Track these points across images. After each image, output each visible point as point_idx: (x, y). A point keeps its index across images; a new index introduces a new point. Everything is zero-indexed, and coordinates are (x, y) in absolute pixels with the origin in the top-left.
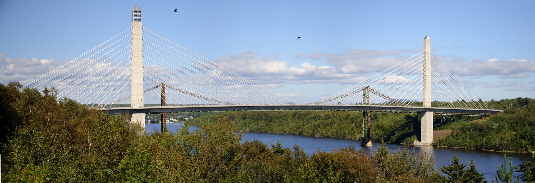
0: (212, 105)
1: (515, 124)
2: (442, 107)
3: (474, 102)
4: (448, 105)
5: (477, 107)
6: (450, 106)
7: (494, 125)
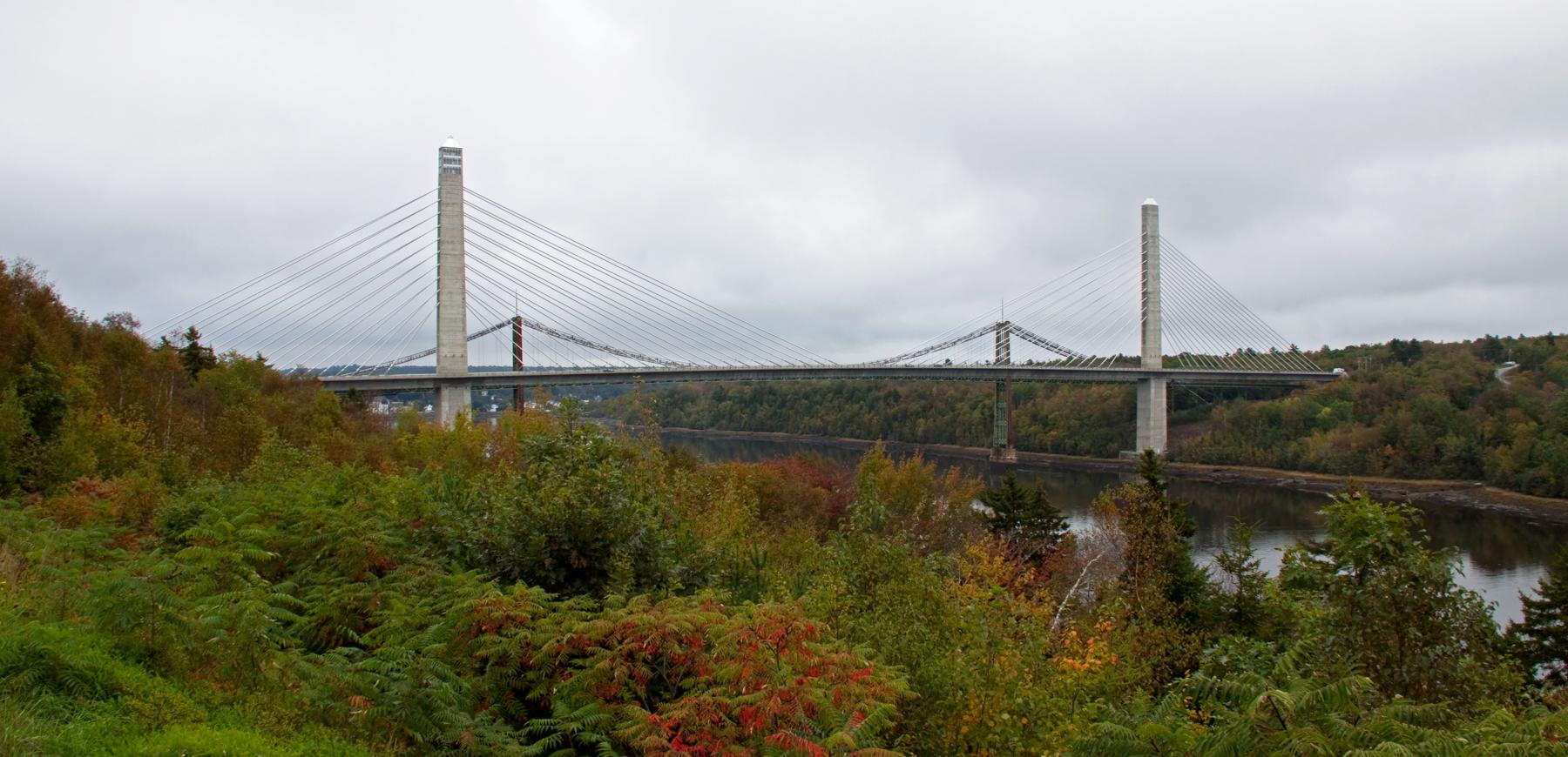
3: (1280, 354)
4: (1205, 361)
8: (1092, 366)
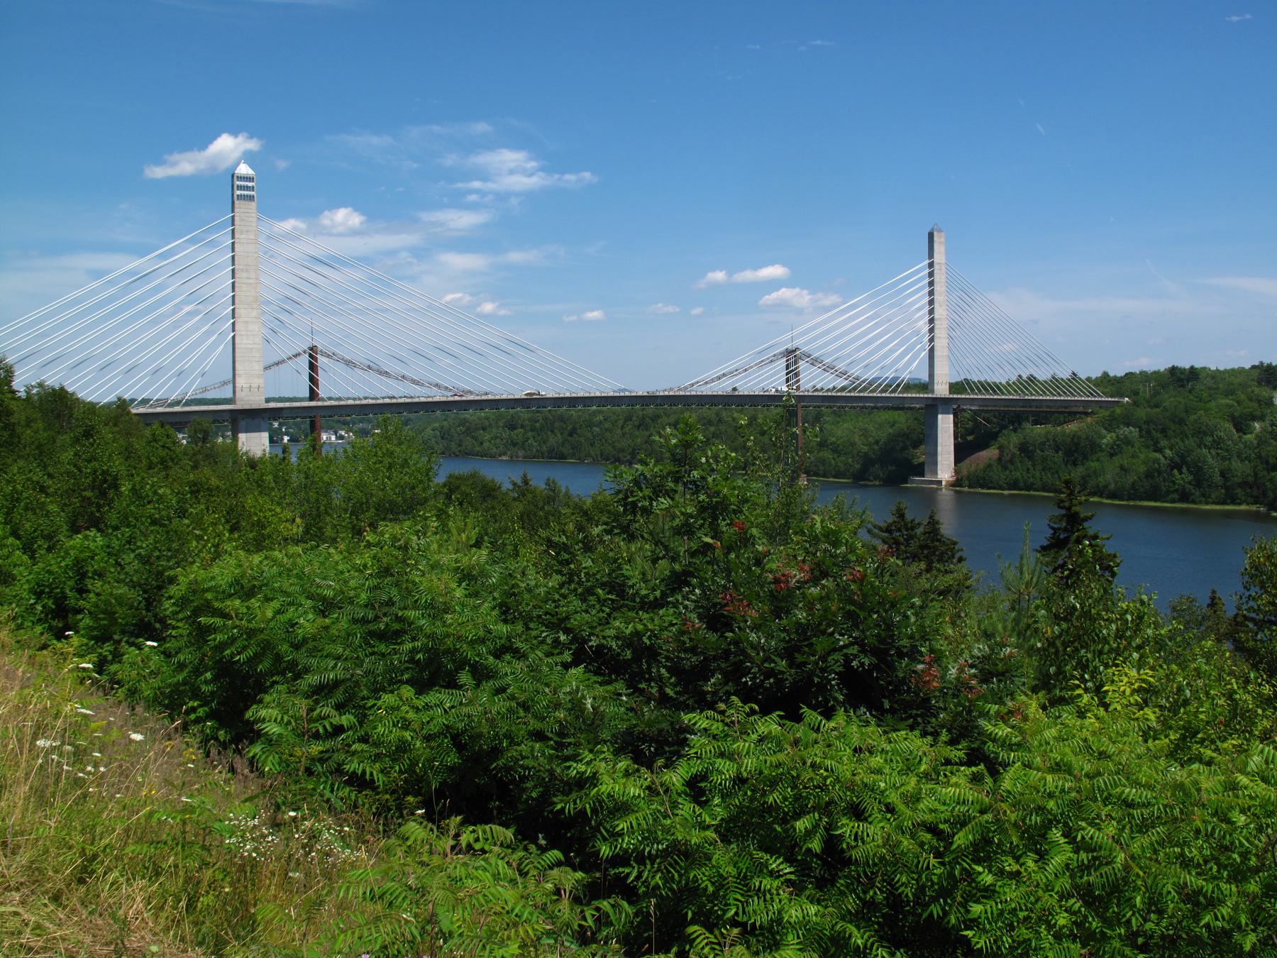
0: (394, 397)
1: (1153, 432)
4: (982, 385)
5: (1065, 393)
6: (994, 391)
7: (1105, 437)
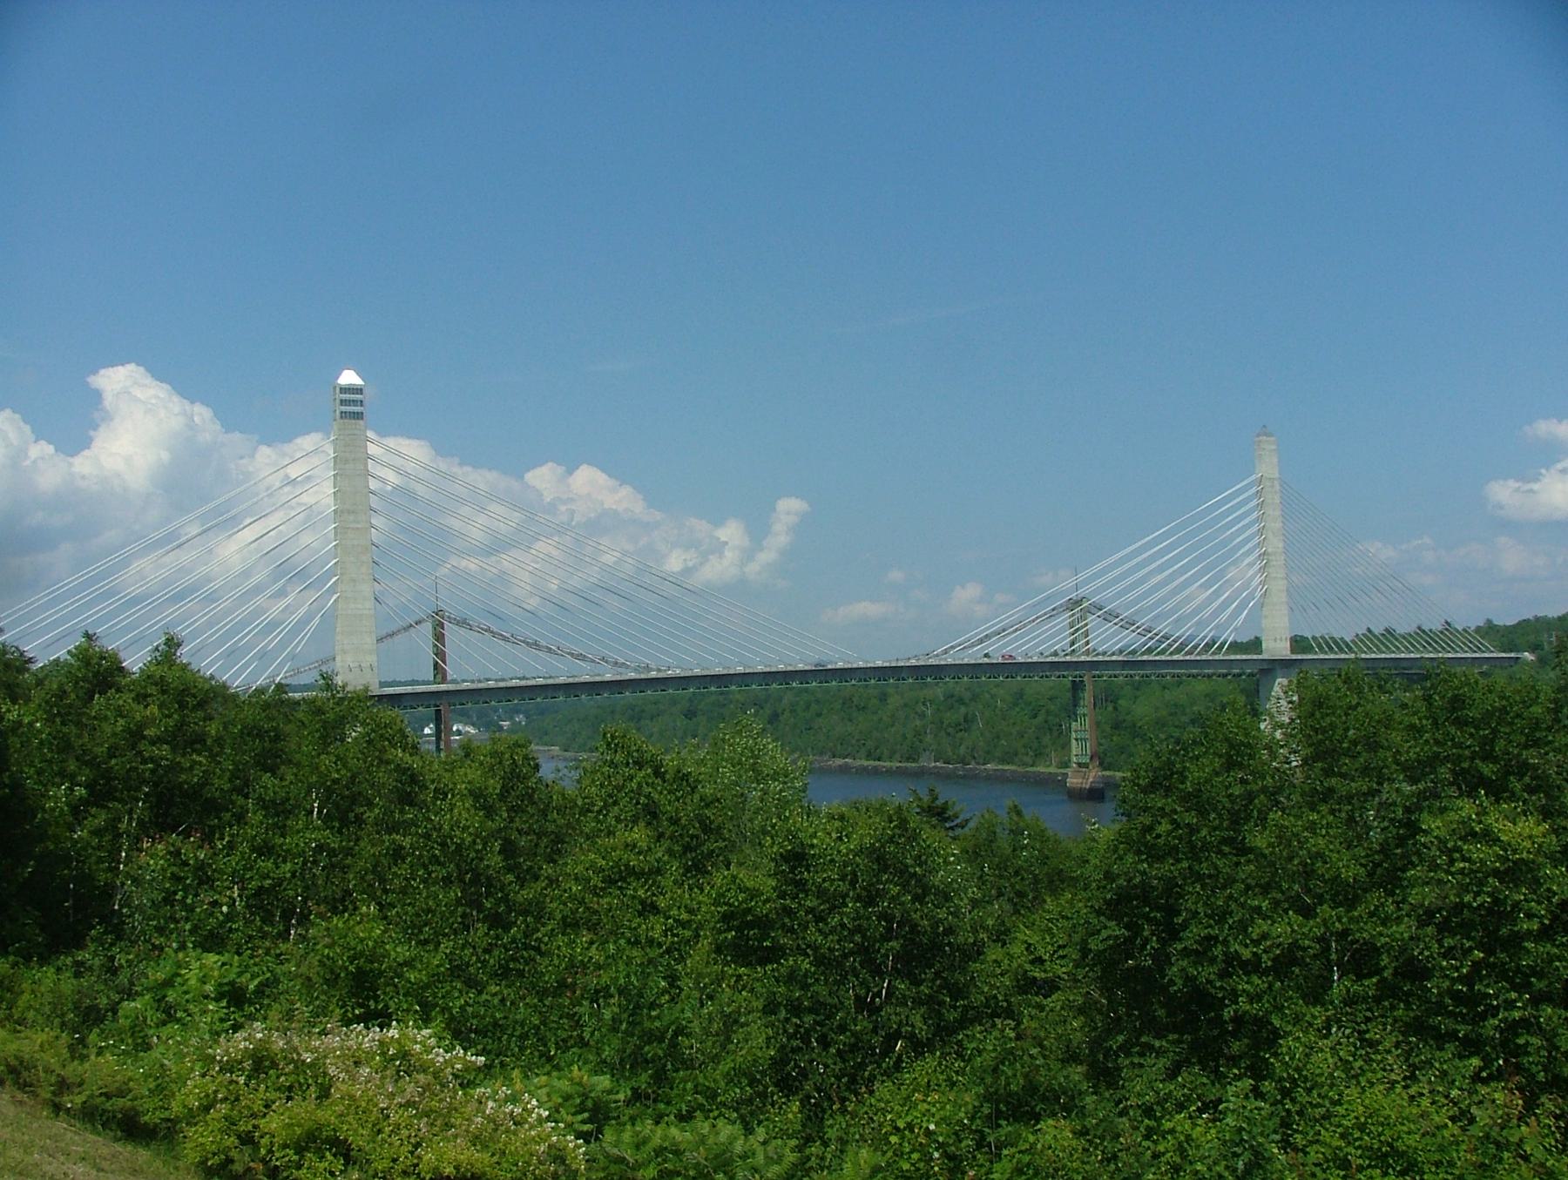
0: (503, 680)
2: (1326, 653)
4: (1347, 645)
8: (1171, 654)
